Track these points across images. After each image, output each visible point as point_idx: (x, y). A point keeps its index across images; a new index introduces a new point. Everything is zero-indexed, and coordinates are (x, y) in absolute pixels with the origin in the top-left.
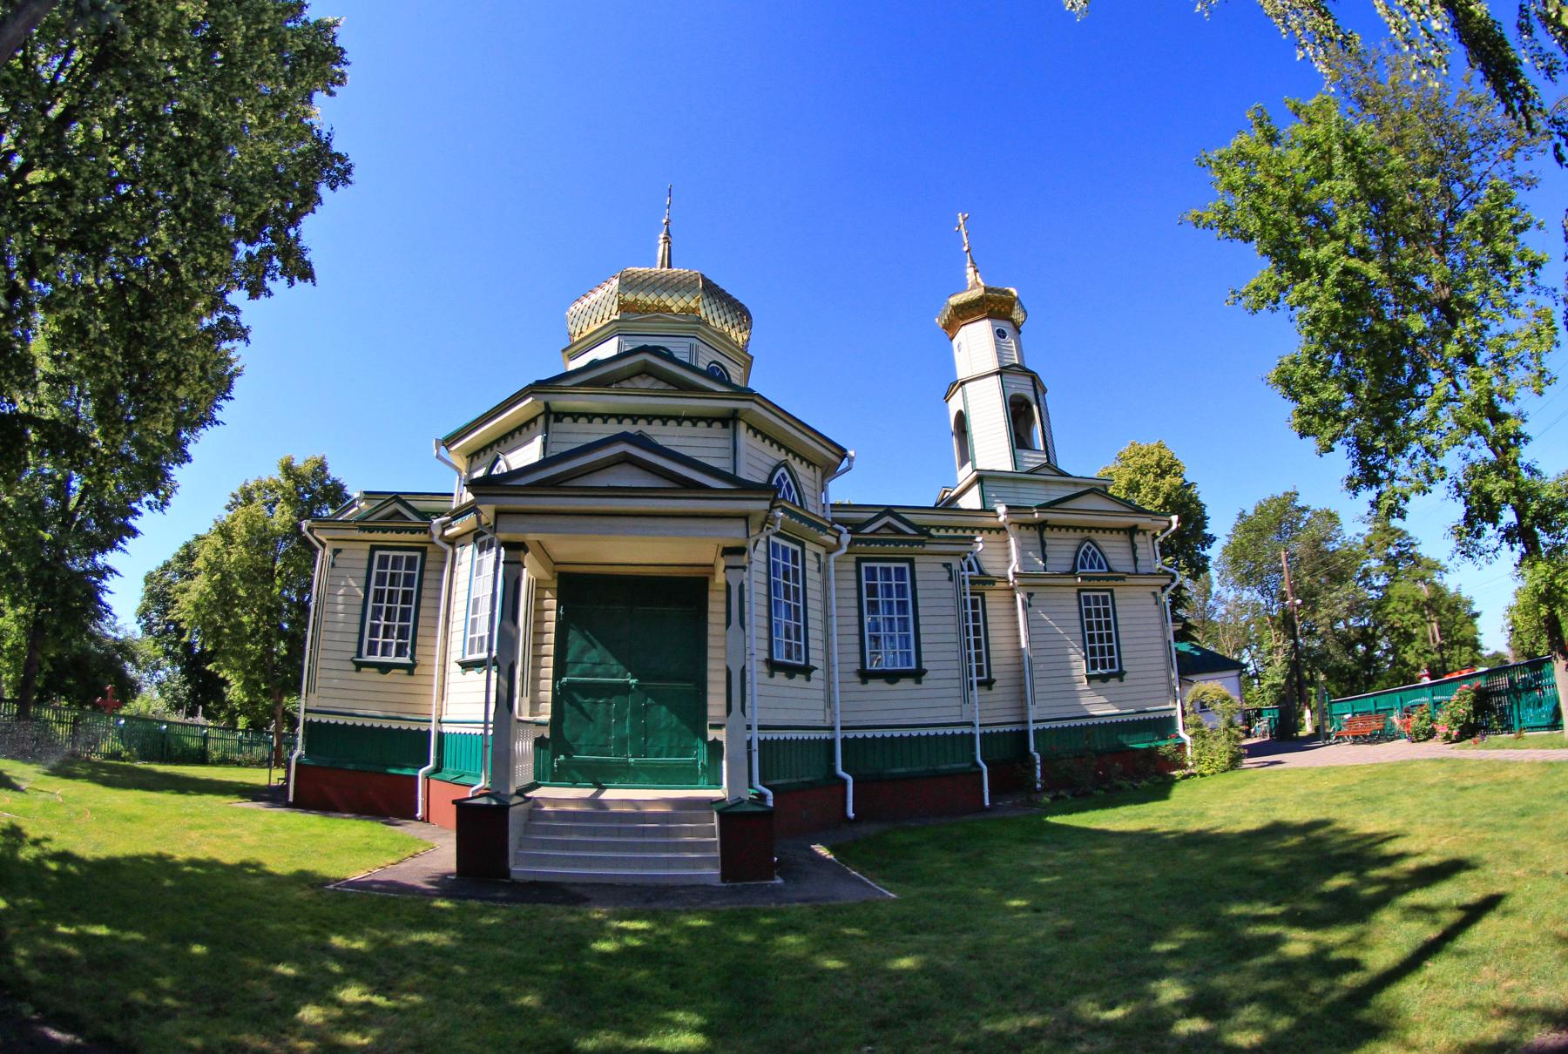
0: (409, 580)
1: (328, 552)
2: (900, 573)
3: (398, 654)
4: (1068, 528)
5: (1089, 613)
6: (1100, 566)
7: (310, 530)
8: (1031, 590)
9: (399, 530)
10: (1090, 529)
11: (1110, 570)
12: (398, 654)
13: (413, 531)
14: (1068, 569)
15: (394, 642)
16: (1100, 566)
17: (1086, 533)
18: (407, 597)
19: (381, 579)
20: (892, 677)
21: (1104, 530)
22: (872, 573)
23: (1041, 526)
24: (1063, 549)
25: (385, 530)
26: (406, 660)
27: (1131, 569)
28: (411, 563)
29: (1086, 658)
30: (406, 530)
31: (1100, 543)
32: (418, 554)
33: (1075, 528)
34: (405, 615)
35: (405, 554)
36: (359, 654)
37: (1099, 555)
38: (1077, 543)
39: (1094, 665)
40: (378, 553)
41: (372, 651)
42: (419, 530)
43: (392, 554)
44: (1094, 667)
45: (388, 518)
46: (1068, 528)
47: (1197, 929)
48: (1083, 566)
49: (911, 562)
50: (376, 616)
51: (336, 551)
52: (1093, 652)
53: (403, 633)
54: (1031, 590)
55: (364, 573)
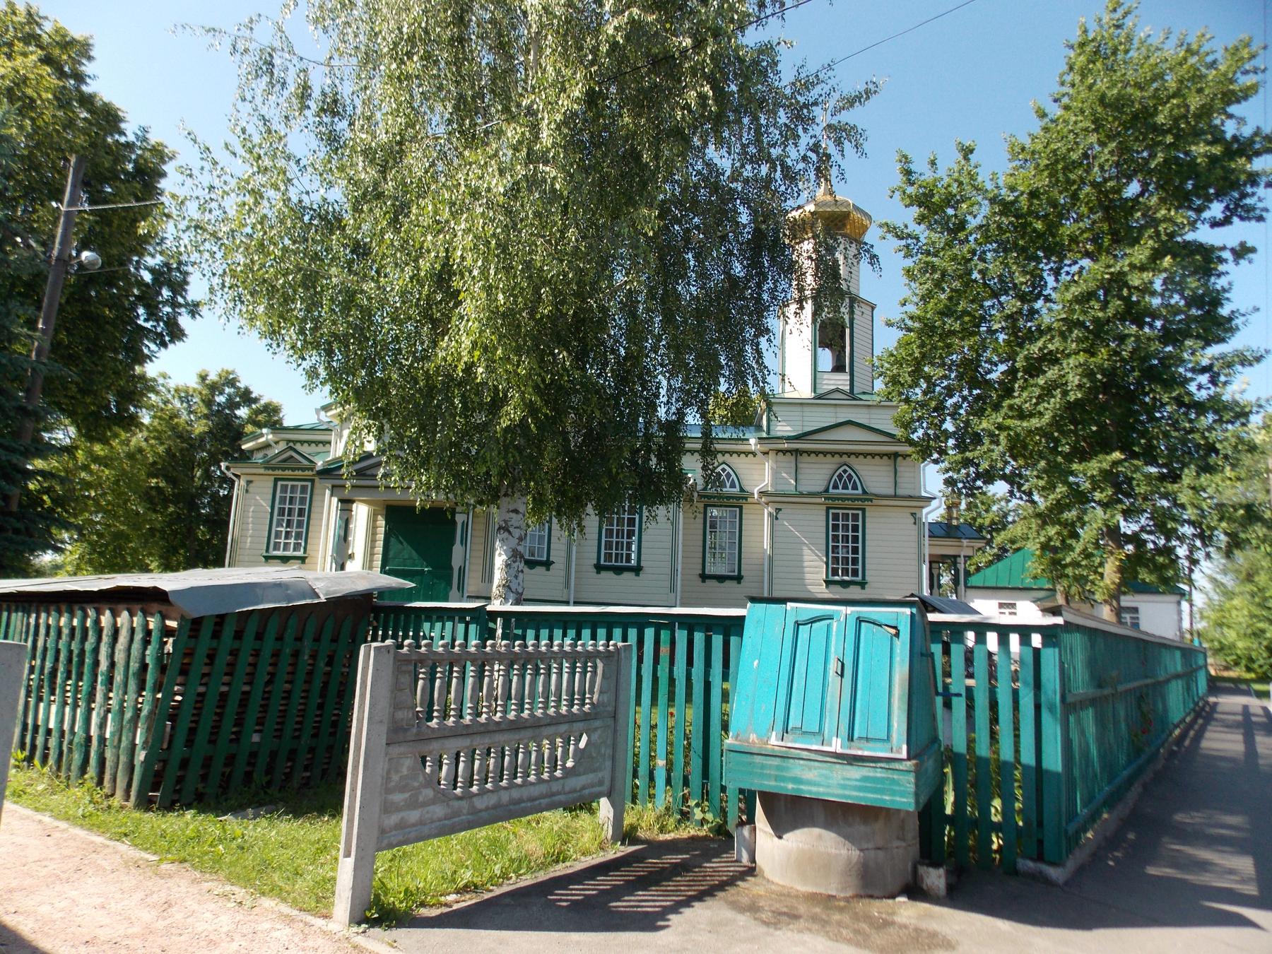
0: (303, 501)
1: (243, 483)
2: (855, 517)
3: (284, 550)
4: (825, 453)
5: (835, 528)
6: (733, 485)
7: (228, 468)
8: (779, 506)
9: (293, 470)
10: (849, 454)
11: (864, 492)
12: (284, 550)
13: (303, 469)
14: (821, 489)
15: (292, 541)
16: (855, 488)
17: (845, 458)
18: (301, 512)
19: (283, 500)
20: (721, 579)
21: (865, 455)
22: (836, 517)
23: (797, 453)
24: (816, 475)
25: (284, 469)
26: (300, 553)
27: (891, 492)
28: (304, 489)
29: (827, 564)
30: (298, 469)
31: (856, 467)
32: (309, 484)
33: (833, 454)
34: (300, 524)
35: (299, 484)
36: (267, 550)
37: (733, 476)
38: (835, 467)
39: (835, 572)
40: (280, 483)
41: (277, 547)
42: (308, 469)
43: (290, 483)
44: (835, 572)
45: (285, 461)
46: (825, 453)
47: (1102, 757)
48: (836, 487)
49: (864, 511)
50: (279, 525)
51: (249, 482)
52: (836, 560)
53: (298, 536)
54: (779, 506)
55: (270, 497)
